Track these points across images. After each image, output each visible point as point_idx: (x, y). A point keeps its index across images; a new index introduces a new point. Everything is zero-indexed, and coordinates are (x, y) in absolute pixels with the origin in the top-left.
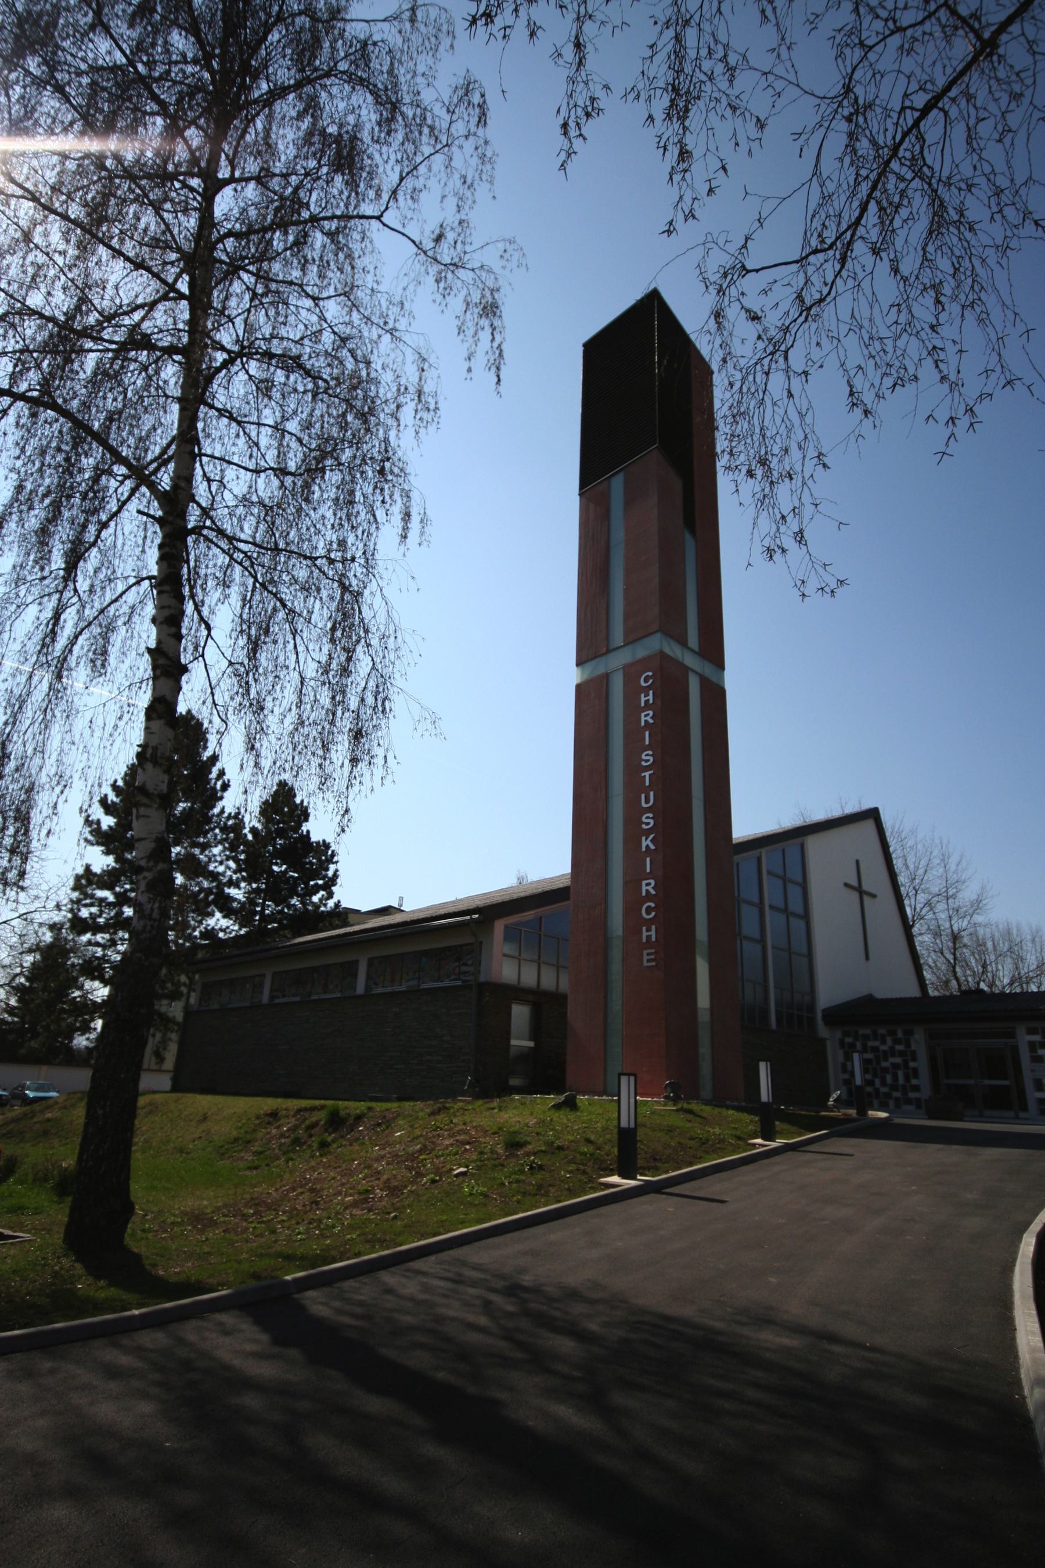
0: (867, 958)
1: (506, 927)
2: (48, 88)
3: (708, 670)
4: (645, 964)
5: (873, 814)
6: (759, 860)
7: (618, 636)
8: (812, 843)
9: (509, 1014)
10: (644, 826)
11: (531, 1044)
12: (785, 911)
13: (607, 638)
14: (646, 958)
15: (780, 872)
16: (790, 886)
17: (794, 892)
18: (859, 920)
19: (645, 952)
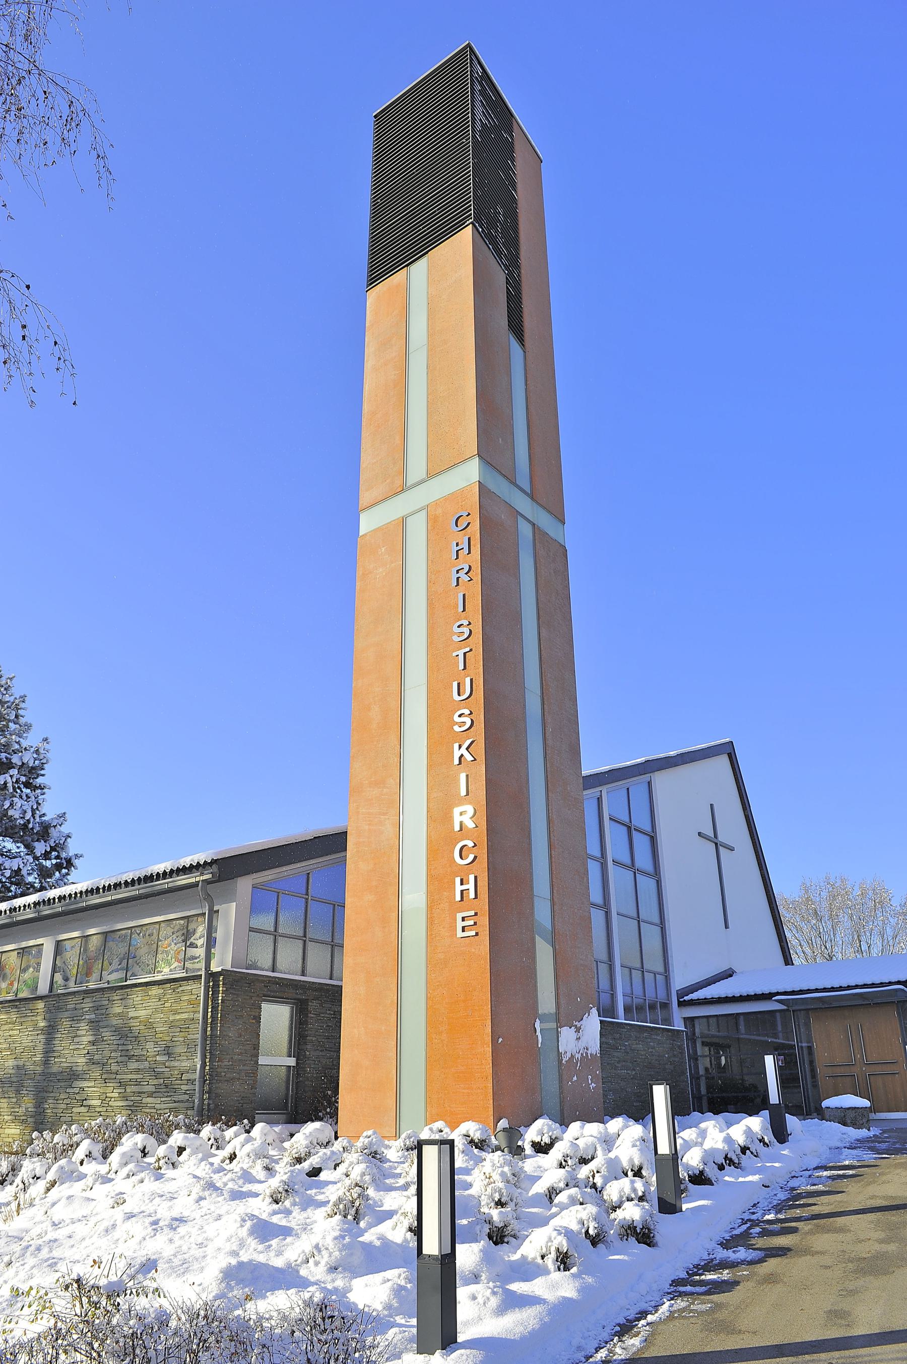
0: (727, 927)
1: (254, 887)
2: (386, 1313)
3: (545, 520)
4: (460, 934)
5: (729, 751)
6: (599, 800)
7: (417, 466)
8: (660, 780)
9: (258, 1019)
10: (457, 728)
11: (292, 1062)
12: (632, 866)
13: (404, 471)
14: (460, 924)
15: (626, 819)
16: (636, 836)
17: (641, 843)
18: (639, 949)
19: (459, 916)
